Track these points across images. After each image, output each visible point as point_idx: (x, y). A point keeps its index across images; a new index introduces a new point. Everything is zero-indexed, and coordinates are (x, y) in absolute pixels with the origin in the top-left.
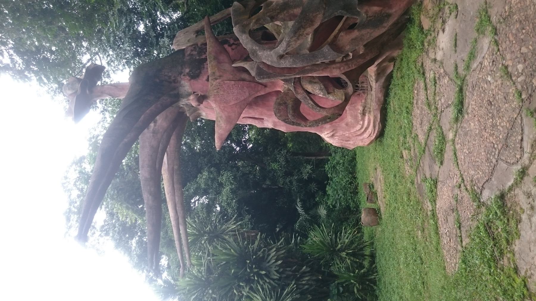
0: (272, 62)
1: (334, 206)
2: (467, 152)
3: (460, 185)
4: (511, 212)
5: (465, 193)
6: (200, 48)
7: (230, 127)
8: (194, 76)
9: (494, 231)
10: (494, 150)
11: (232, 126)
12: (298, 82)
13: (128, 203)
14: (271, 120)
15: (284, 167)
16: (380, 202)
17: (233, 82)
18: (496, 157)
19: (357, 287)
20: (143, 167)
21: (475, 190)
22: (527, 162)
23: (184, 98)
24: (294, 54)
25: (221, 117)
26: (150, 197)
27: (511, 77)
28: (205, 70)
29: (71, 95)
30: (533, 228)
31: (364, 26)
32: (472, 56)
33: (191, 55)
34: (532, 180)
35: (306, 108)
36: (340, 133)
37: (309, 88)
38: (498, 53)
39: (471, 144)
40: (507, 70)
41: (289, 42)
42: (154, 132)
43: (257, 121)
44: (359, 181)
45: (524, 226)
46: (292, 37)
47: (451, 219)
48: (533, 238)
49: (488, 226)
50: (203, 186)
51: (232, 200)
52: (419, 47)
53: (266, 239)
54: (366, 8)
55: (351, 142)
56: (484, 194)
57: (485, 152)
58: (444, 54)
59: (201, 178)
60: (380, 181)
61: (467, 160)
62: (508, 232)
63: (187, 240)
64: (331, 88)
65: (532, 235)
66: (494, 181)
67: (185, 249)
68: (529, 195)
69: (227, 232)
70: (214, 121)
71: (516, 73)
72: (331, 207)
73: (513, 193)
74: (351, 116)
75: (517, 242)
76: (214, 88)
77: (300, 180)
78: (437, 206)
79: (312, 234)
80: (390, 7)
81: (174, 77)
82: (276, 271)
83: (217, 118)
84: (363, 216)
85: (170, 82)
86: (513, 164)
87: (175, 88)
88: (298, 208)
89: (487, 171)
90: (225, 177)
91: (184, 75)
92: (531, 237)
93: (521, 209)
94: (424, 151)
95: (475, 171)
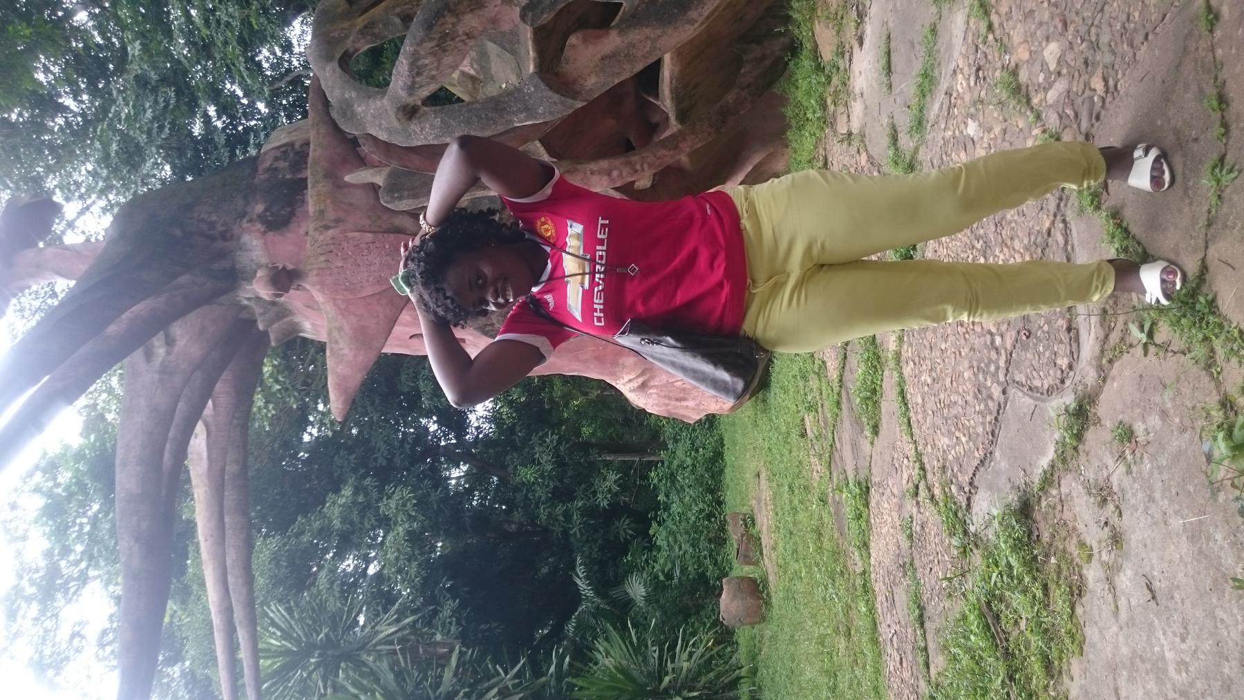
0: (390, 131)
1: (669, 576)
2: (929, 381)
3: (917, 487)
4: (1053, 560)
5: (930, 513)
6: (297, 153)
7: (366, 359)
8: (277, 222)
9: (1009, 628)
10: (993, 355)
11: (372, 357)
16: (766, 561)
17: (370, 235)
18: (1002, 378)
20: (124, 464)
21: (952, 497)
22: (1091, 377)
25: (340, 329)
26: (136, 548)
27: (1029, 101)
30: (1123, 615)
32: (928, 80)
33: (273, 170)
34: (1109, 437)
38: (991, 37)
39: (937, 353)
40: (1017, 80)
42: (164, 370)
44: (728, 510)
45: (1094, 606)
46: (422, 41)
47: (901, 597)
48: (1124, 650)
49: (991, 614)
50: (337, 523)
51: (409, 561)
52: (814, 112)
53: (481, 659)
55: (691, 404)
56: (975, 508)
57: (971, 367)
58: (866, 107)
59: (334, 503)
60: (766, 505)
61: (930, 405)
62: (1046, 631)
65: (1121, 639)
66: (1001, 461)
68: (1103, 494)
69: (375, 645)
71: (1041, 78)
72: (662, 578)
73: (1054, 492)
75: (1076, 666)
76: (319, 251)
77: (591, 512)
78: (872, 561)
79: (601, 649)
81: (225, 224)
83: (330, 334)
85: (213, 238)
86: (1050, 391)
87: (223, 255)
88: (578, 581)
89: (980, 430)
90: (397, 500)
91: (250, 221)
92: (1116, 647)
93: (1082, 545)
94: (838, 403)
95: (951, 434)
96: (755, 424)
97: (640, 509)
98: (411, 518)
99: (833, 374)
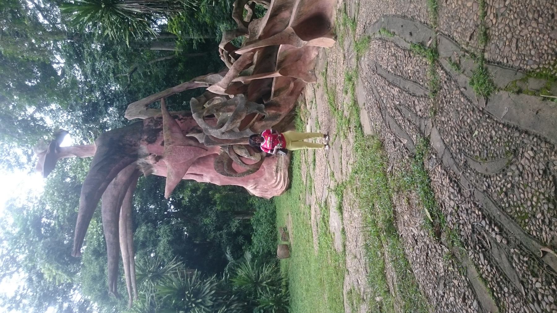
1: (258, 252)
7: (177, 181)
8: (151, 141)
11: (180, 180)
12: (231, 148)
13: (59, 262)
14: (209, 176)
15: (215, 222)
19: (275, 309)
20: (105, 212)
23: (141, 158)
24: (231, 131)
25: (172, 172)
26: (111, 236)
28: (160, 137)
29: (41, 154)
31: (268, 119)
35: (237, 166)
36: (261, 186)
37: (238, 152)
41: (228, 126)
43: (197, 177)
50: (141, 239)
54: (268, 111)
55: (269, 193)
63: (135, 278)
64: (253, 152)
67: (133, 285)
70: (164, 178)
74: (268, 173)
80: (281, 111)
82: (211, 300)
83: (168, 174)
87: (135, 150)
96: (287, 199)
97: (246, 233)
98: (168, 236)
99: (305, 184)
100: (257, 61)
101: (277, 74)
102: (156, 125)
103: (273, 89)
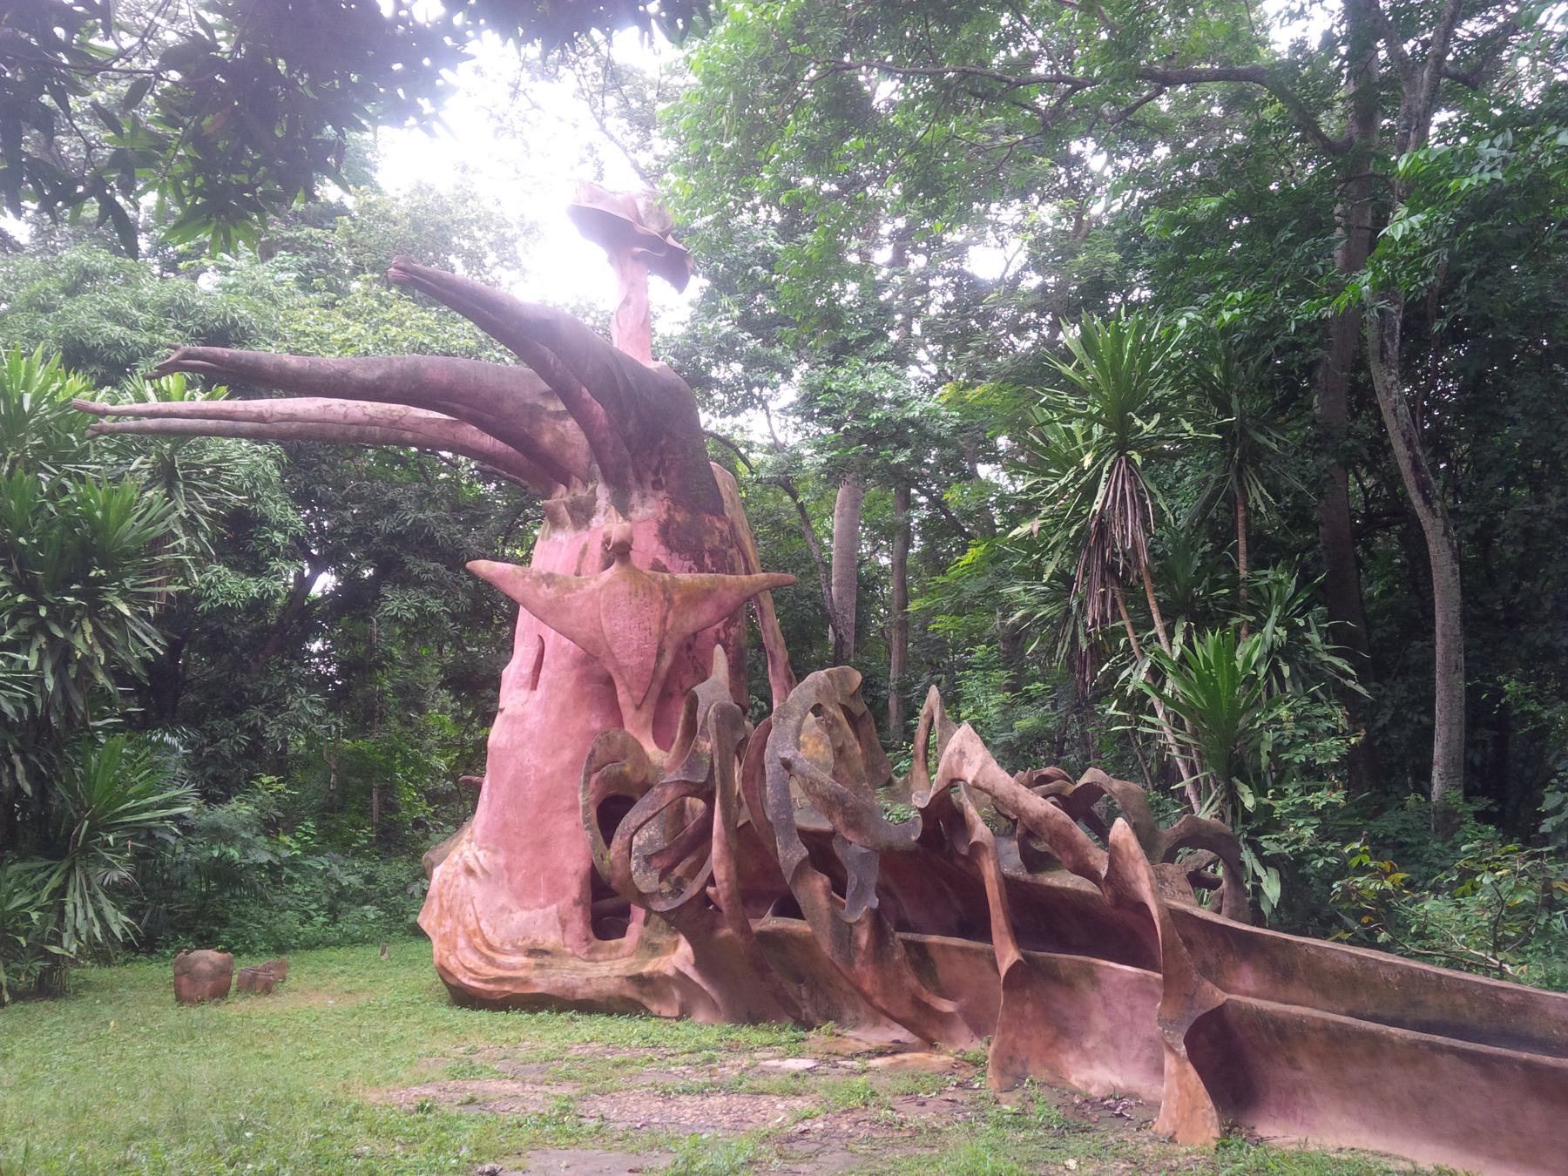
8: (666, 532)
17: (245, 443)
43: (527, 671)
84: (213, 955)
85: (656, 473)
100: (1051, 888)
101: (1008, 955)
102: (713, 553)
103: (934, 939)
